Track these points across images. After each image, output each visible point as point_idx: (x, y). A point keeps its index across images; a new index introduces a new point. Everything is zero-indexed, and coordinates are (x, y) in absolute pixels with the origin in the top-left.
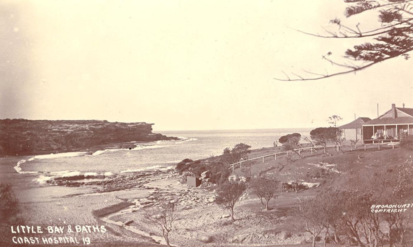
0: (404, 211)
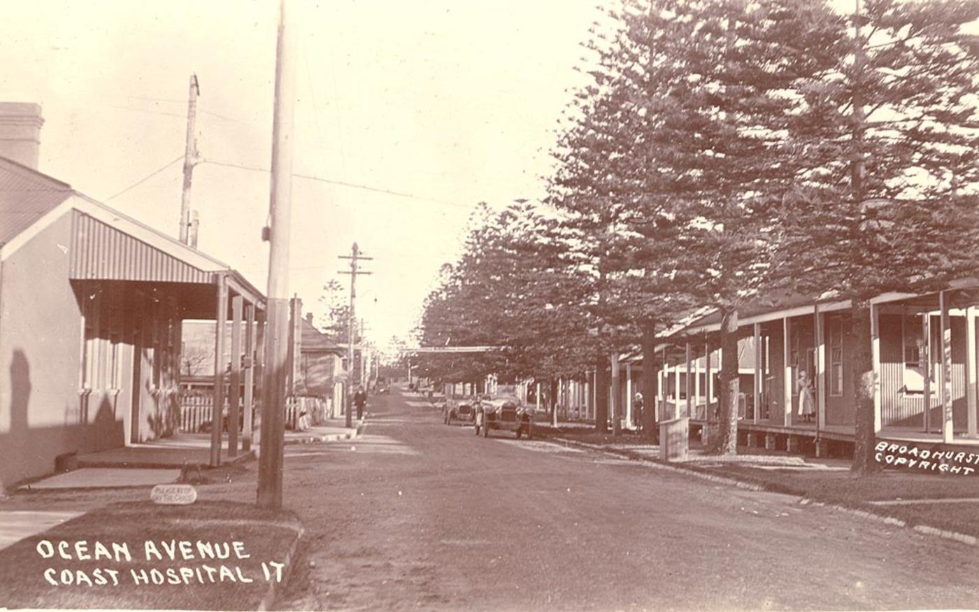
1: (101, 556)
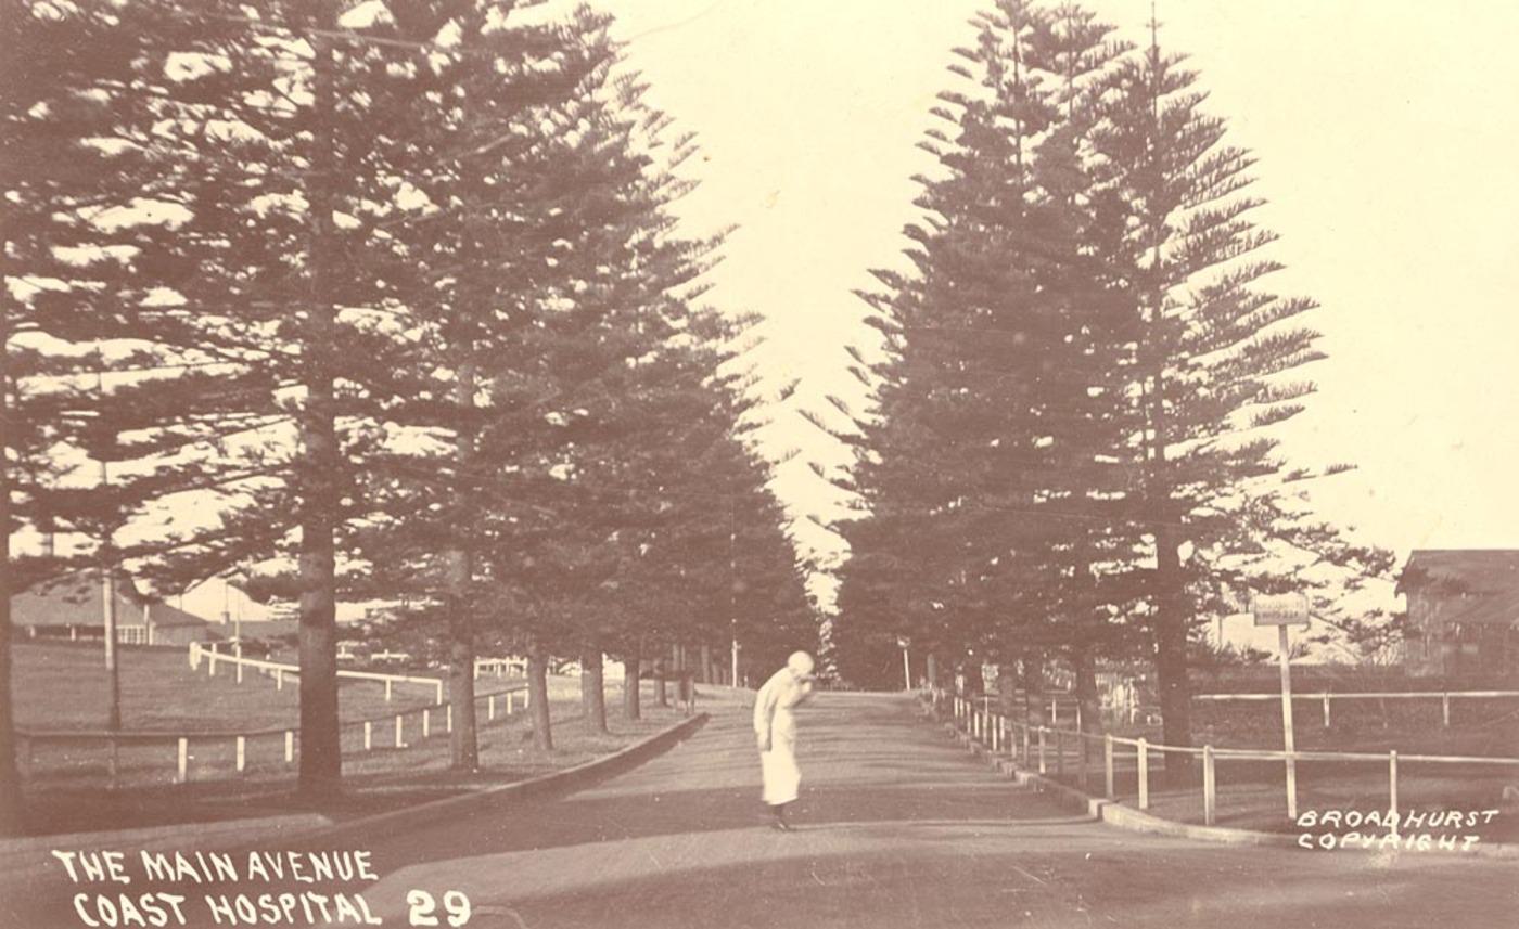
0: (1487, 821)
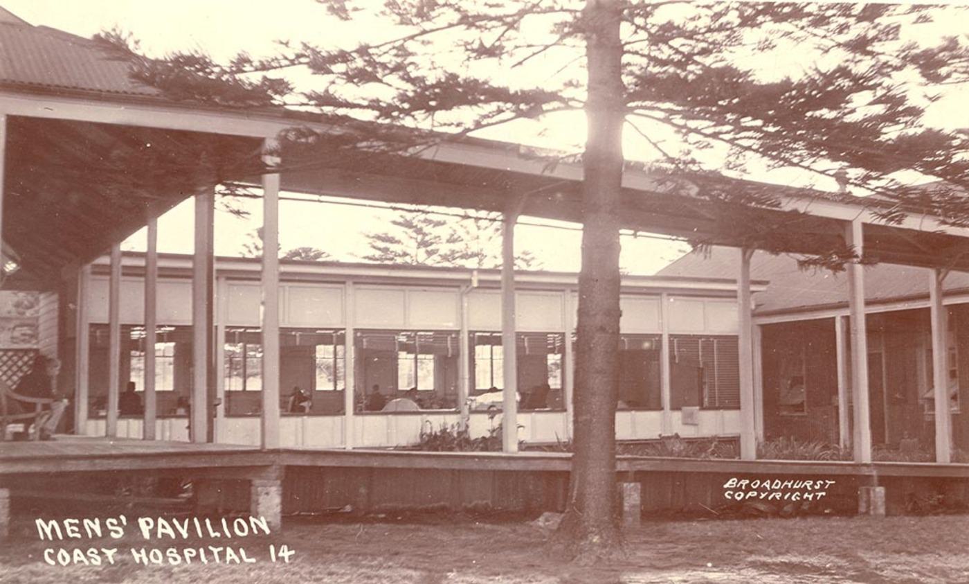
0: (818, 498)
1: (163, 534)
